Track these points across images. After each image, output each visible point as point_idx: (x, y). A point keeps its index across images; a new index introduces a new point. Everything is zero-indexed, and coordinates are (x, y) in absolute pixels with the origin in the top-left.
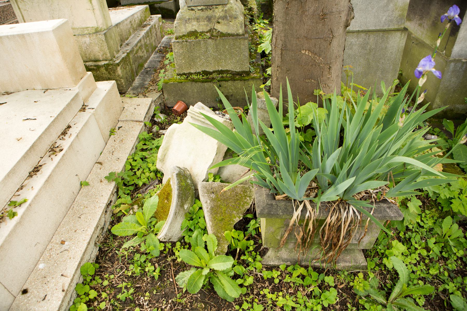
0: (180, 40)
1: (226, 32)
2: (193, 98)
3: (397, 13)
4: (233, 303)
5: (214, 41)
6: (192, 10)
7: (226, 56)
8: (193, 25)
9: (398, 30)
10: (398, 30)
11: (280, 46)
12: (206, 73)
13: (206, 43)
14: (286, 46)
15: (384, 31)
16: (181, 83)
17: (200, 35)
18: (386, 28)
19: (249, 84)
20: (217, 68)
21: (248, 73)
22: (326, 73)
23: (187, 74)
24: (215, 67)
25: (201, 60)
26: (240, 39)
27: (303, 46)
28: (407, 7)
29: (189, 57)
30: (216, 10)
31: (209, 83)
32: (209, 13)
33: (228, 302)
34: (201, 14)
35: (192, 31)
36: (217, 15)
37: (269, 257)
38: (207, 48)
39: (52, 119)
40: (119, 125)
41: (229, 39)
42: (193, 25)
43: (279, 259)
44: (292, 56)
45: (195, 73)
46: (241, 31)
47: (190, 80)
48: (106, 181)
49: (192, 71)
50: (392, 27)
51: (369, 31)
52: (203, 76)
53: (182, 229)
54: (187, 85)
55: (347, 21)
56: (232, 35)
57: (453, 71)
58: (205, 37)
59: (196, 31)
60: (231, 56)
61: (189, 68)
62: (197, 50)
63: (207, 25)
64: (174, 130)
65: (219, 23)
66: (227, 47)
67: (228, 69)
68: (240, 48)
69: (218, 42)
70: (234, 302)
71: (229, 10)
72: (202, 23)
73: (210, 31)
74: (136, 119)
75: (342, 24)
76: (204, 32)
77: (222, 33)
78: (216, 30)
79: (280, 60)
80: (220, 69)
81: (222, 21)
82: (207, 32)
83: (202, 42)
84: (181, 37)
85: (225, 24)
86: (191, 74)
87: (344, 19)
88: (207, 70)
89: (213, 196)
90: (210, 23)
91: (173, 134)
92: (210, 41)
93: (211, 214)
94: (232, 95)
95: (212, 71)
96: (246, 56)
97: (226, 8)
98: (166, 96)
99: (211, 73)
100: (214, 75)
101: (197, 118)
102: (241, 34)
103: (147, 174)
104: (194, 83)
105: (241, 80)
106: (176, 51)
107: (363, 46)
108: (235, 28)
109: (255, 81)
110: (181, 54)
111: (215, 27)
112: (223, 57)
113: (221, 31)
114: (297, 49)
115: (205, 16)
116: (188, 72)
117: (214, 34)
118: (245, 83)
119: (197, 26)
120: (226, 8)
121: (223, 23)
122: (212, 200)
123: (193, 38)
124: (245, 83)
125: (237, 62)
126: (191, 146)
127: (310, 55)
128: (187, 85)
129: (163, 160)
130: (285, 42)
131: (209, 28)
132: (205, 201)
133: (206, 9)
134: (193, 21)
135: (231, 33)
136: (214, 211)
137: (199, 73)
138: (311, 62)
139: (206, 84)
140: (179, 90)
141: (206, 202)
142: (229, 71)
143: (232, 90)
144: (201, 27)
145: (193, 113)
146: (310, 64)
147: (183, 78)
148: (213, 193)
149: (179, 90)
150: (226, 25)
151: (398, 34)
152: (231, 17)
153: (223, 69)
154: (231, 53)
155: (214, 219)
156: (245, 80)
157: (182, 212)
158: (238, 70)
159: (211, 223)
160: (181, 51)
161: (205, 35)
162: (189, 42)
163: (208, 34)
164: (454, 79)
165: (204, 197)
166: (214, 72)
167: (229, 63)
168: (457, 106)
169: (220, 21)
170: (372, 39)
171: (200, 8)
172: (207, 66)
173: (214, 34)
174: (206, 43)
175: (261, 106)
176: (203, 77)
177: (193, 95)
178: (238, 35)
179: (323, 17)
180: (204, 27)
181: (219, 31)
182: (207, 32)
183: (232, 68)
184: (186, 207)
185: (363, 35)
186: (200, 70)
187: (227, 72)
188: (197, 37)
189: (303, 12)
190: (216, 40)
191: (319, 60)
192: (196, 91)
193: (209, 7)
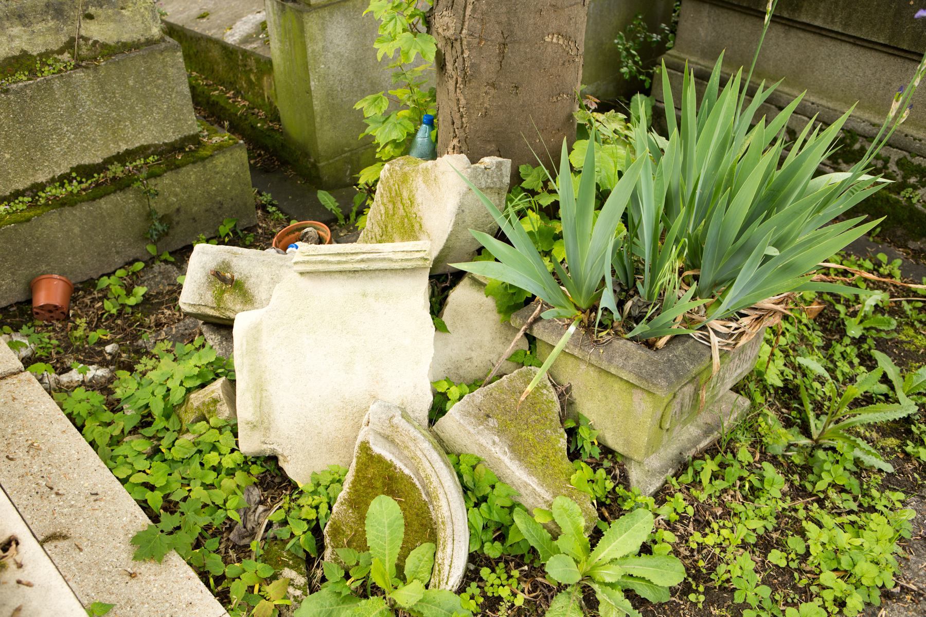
1: (115, 39)
2: (74, 255)
4: (673, 599)
5: (91, 72)
7: (132, 108)
8: (11, 38)
12: (85, 171)
13: (67, 84)
16: (28, 220)
17: (44, 64)
19: (216, 166)
20: (113, 150)
21: (195, 139)
23: (25, 191)
24: (107, 147)
25: (61, 136)
26: (161, 52)
27: (548, 26)
29: (23, 137)
31: (112, 196)
33: (666, 603)
35: (14, 57)
37: (638, 482)
38: (74, 98)
41: (133, 59)
42: (11, 38)
43: (653, 475)
44: (525, 53)
45: (52, 181)
47: (46, 205)
48: (146, 569)
49: (41, 178)
52: (80, 182)
54: (49, 223)
58: (60, 66)
59: (24, 54)
60: (147, 104)
61: (30, 172)
62: (44, 110)
63: (58, 31)
65: (90, 17)
66: (131, 83)
67: (143, 142)
68: (165, 77)
69: (102, 73)
70: (673, 596)
73: (70, 45)
76: (53, 52)
77: (104, 46)
78: (86, 39)
80: (123, 147)
81: (100, 11)
82: (61, 51)
83: (57, 84)
85: (108, 18)
86: (42, 187)
88: (86, 161)
89: (492, 422)
90: (65, 23)
91: (257, 339)
92: (80, 74)
93: (520, 460)
94: (178, 210)
95: (101, 161)
96: (185, 96)
99: (102, 168)
101: (321, 267)
102: (157, 37)
104: (67, 211)
105: (194, 163)
108: (139, 25)
109: (228, 154)
111: (83, 33)
112: (124, 113)
113: (101, 39)
114: (537, 36)
116: (29, 184)
118: (204, 167)
119: (25, 37)
121: (102, 18)
123: (22, 76)
124: (204, 167)
125: (166, 117)
127: (561, 42)
128: (49, 223)
130: (510, 24)
131: (64, 39)
132: (491, 443)
134: (7, 24)
135: (130, 41)
138: (561, 57)
139: (102, 201)
140: (26, 244)
141: (494, 443)
142: (149, 147)
143: (176, 195)
144: (40, 40)
145: (320, 258)
146: (561, 62)
147: (20, 207)
148: (488, 416)
149: (26, 244)
150: (114, 21)
153: (131, 147)
154: (145, 97)
156: (203, 159)
158: (172, 137)
159: (534, 479)
161: (56, 61)
162: (16, 92)
163: (66, 56)
165: (482, 435)
166: (109, 161)
167: (144, 126)
169: (92, 10)
172: (85, 150)
173: (84, 52)
174: (67, 84)
175: (487, 182)
176: (83, 186)
177: (72, 246)
178: (150, 42)
180: (50, 38)
181: (96, 42)
182: (61, 51)
183: (155, 138)
186: (64, 169)
187: (142, 151)
190: (96, 68)
192: (77, 230)
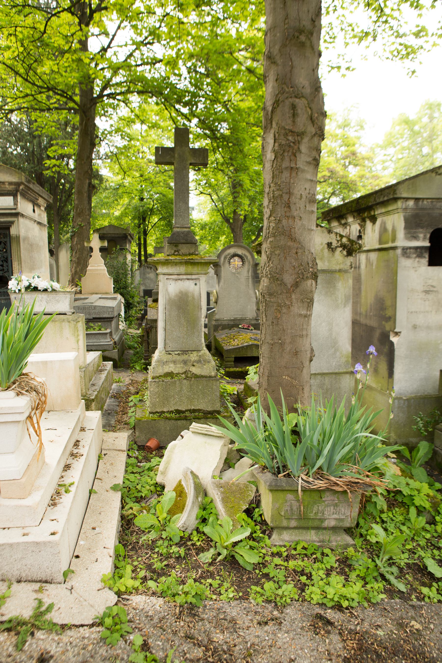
0: (157, 380)
3: (343, 360)
6: (170, 354)
9: (347, 373)
10: (347, 373)
11: (267, 374)
12: (178, 412)
14: (271, 373)
15: (336, 374)
18: (337, 371)
22: (301, 392)
25: (175, 398)
28: (350, 355)
30: (192, 355)
32: (185, 357)
34: (178, 358)
36: (193, 359)
38: (181, 388)
39: (71, 430)
40: (104, 452)
45: (168, 412)
46: (213, 374)
50: (341, 371)
51: (324, 374)
53: (197, 519)
55: (311, 357)
56: (205, 377)
57: (399, 407)
59: (172, 372)
63: (183, 368)
64: (175, 445)
65: (194, 366)
67: (200, 408)
68: (212, 389)
71: (203, 355)
72: (179, 366)
73: (185, 372)
74: (118, 448)
75: (308, 359)
77: (196, 375)
79: (267, 384)
80: (193, 408)
83: (178, 382)
84: (158, 377)
85: (199, 367)
86: (163, 412)
87: (309, 355)
97: (200, 354)
98: (137, 433)
99: (183, 412)
100: (187, 414)
103: (148, 487)
104: (167, 421)
106: (152, 389)
107: (321, 386)
110: (157, 393)
112: (196, 396)
115: (181, 359)
117: (189, 375)
120: (200, 354)
122: (222, 493)
123: (169, 378)
126: (194, 456)
129: (163, 473)
133: (182, 354)
136: (225, 500)
137: (172, 412)
151: (348, 376)
152: (204, 361)
155: (225, 506)
157: (197, 503)
158: (210, 409)
160: (157, 390)
163: (183, 376)
164: (401, 415)
166: (187, 411)
168: (411, 439)
169: (195, 364)
170: (327, 380)
171: (177, 353)
172: (180, 405)
173: (189, 375)
174: (181, 383)
178: (210, 377)
179: (296, 353)
184: (200, 499)
185: (319, 377)
187: (199, 411)
188: (172, 378)
189: (283, 350)
191: (295, 382)
193: (185, 352)
